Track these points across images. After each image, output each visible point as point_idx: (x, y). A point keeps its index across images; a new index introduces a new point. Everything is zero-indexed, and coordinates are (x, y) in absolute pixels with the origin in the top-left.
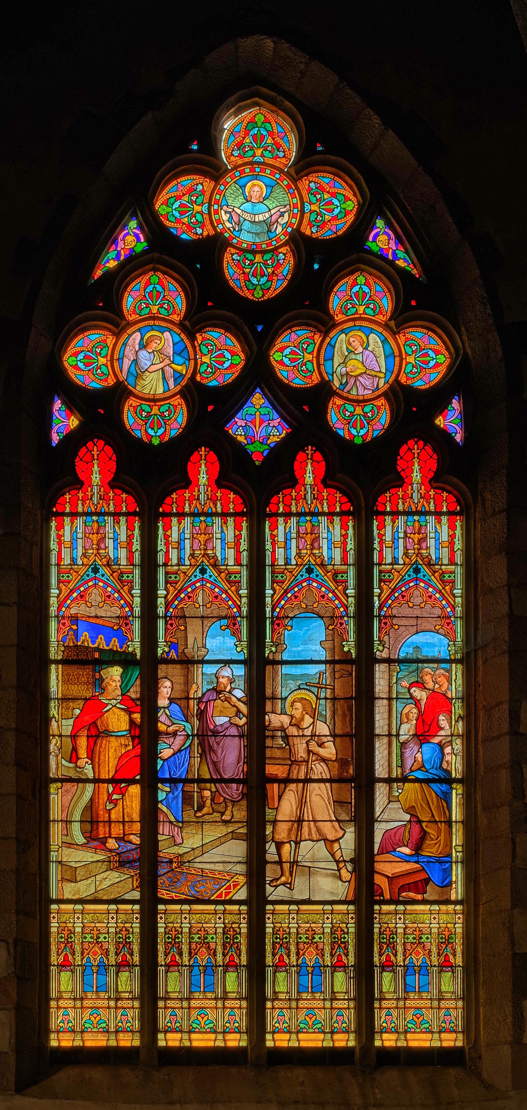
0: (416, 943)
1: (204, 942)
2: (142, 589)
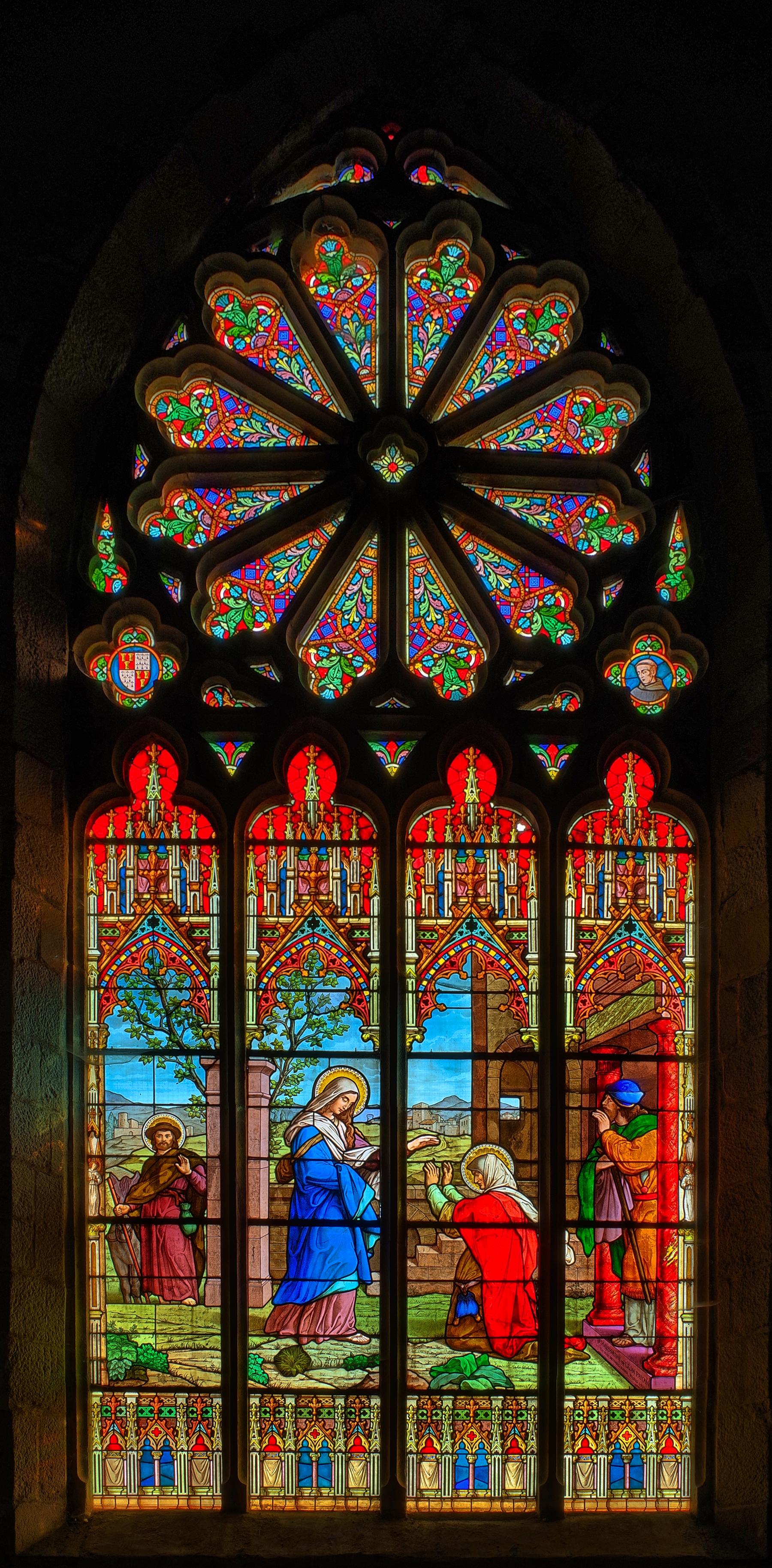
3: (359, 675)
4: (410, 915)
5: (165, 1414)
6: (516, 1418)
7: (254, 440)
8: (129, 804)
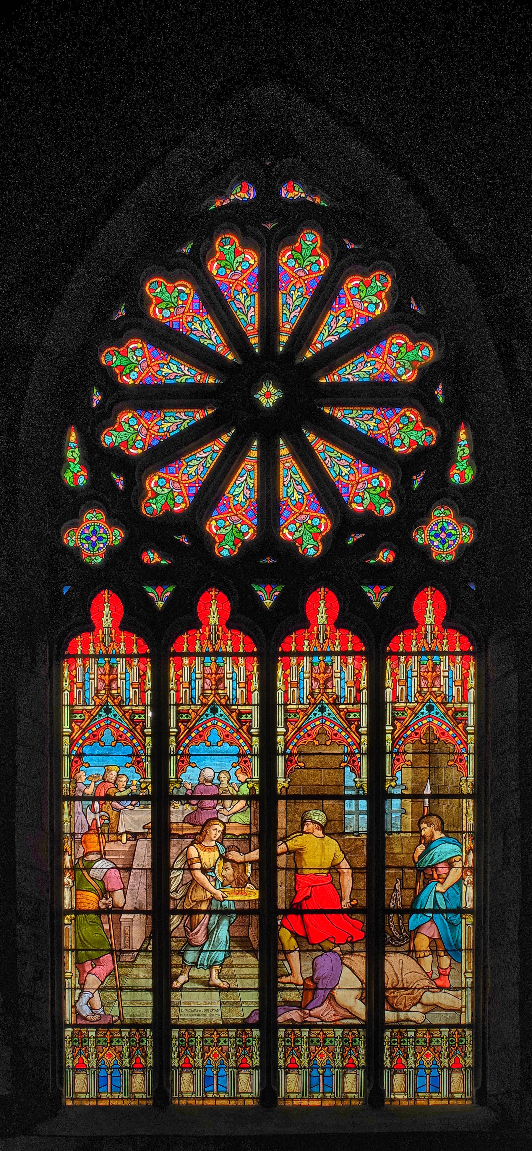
3: (246, 538)
4: (66, 704)
5: (434, 1043)
6: (400, 1043)
7: (172, 377)
8: (307, 627)
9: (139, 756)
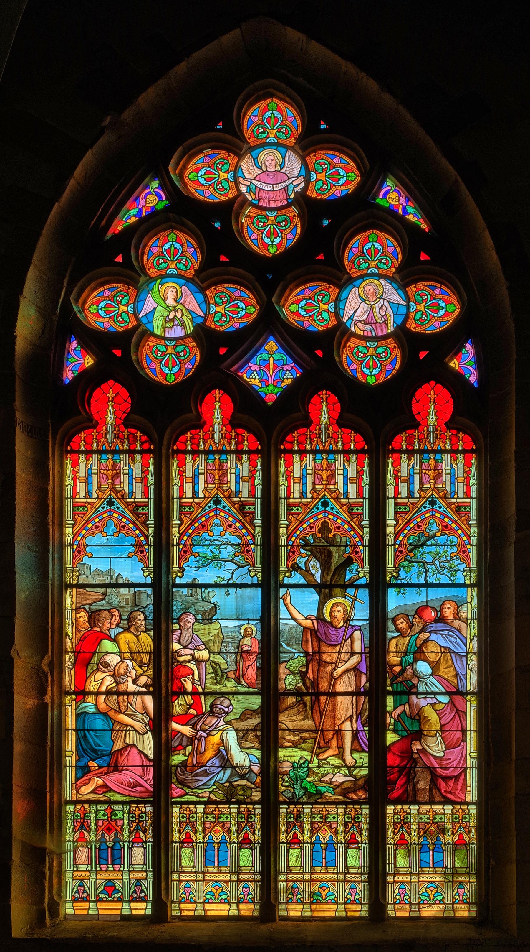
0: (322, 822)
1: (433, 822)
2: (370, 521)
8: (94, 427)
9: (464, 545)
